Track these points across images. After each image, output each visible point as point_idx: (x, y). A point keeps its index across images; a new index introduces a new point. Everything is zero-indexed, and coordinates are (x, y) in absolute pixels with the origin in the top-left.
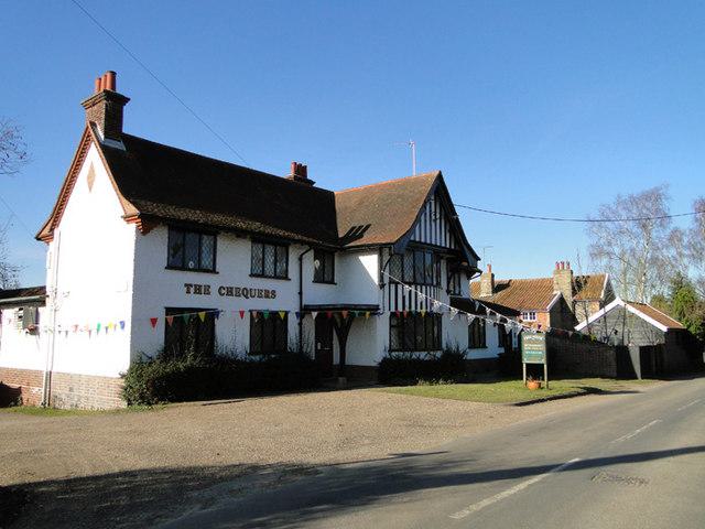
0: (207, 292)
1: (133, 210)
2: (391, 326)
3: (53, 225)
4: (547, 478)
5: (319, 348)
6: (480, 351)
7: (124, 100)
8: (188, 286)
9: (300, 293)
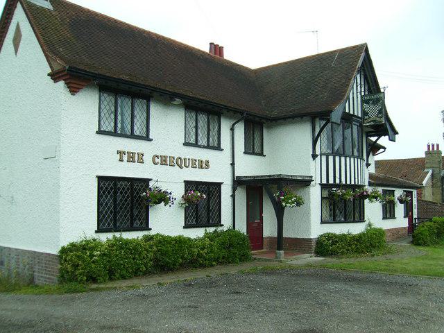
0: (141, 161)
9: (233, 164)
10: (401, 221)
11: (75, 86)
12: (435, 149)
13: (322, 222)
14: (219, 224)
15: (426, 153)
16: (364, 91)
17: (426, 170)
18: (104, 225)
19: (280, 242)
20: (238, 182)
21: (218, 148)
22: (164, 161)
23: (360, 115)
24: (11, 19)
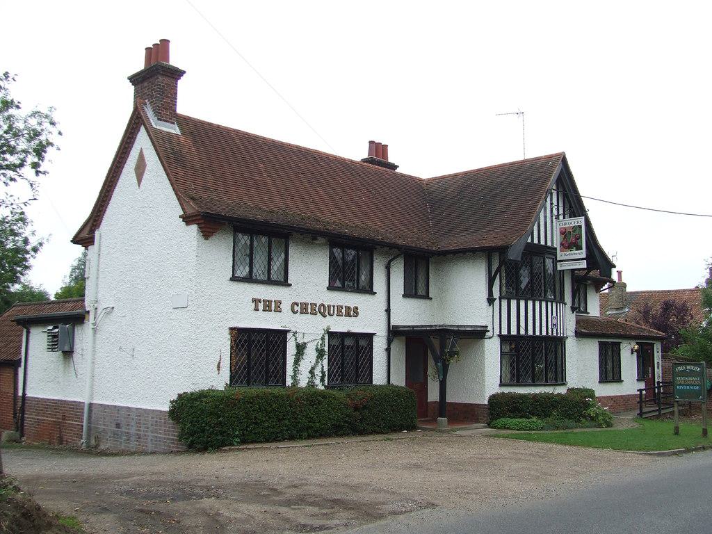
0: (278, 310)
4: (36, 394)
6: (375, 339)
7: (177, 74)
8: (256, 301)
9: (388, 311)
10: (630, 384)
11: (209, 230)
20: (394, 333)
21: (369, 290)
22: (302, 308)
24: (133, 143)
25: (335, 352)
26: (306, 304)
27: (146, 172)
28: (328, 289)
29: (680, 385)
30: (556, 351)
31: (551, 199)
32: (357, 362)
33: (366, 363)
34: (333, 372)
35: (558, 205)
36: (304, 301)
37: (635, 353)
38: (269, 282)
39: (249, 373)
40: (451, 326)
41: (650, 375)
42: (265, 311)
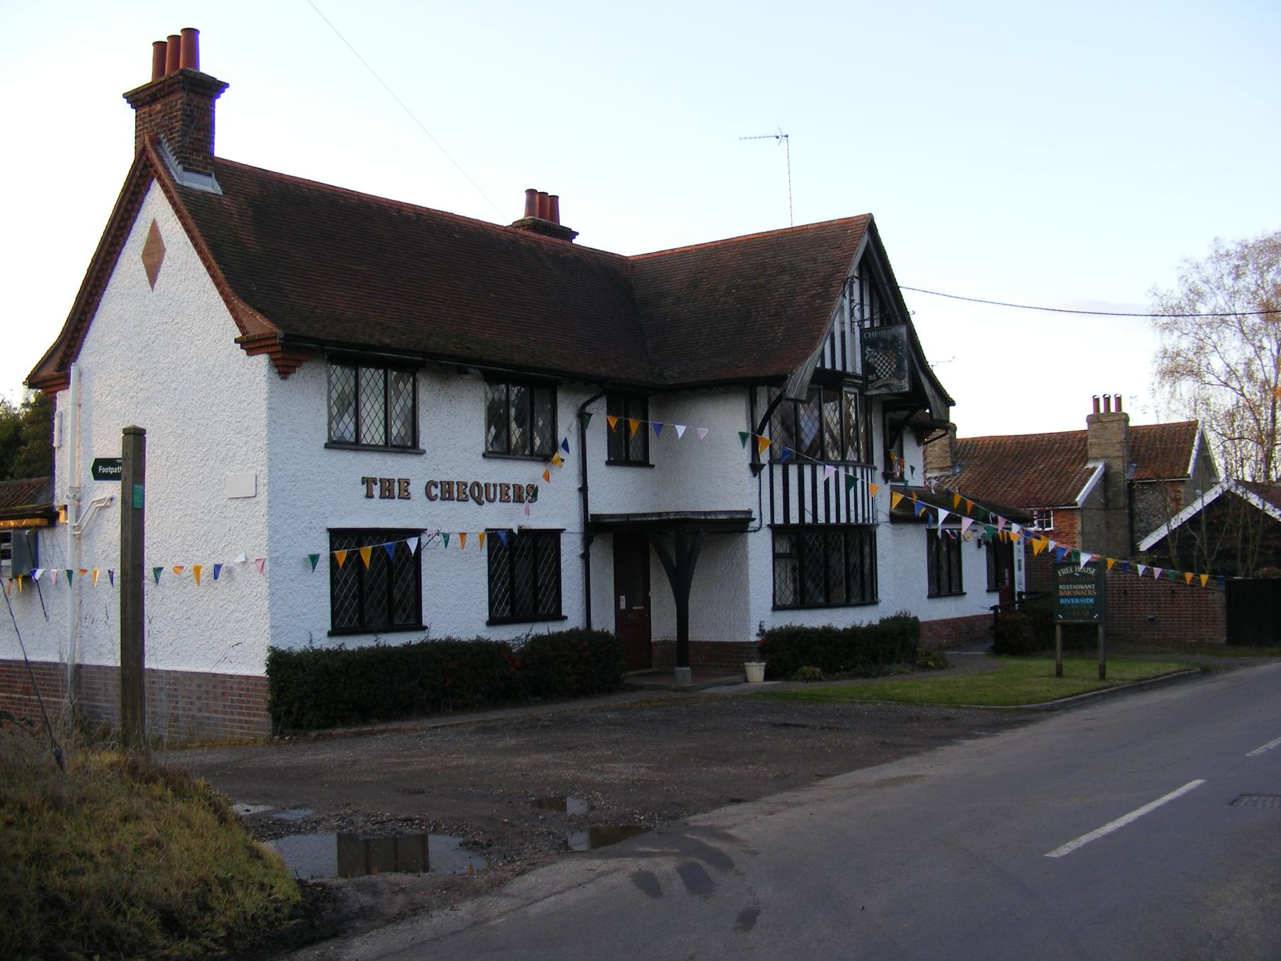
1: (261, 325)
2: (776, 556)
3: (65, 354)
5: (623, 606)
6: (564, 539)
7: (215, 88)
8: (368, 482)
9: (584, 490)
12: (1113, 409)
13: (776, 608)
14: (558, 616)
15: (1091, 420)
16: (872, 319)
17: (1090, 466)
18: (342, 620)
19: (683, 649)
20: (594, 527)
22: (446, 491)
23: (859, 371)
25: (499, 563)
26: (450, 484)
27: (166, 263)
28: (484, 455)
29: (1065, 597)
30: (862, 550)
31: (851, 294)
32: (535, 582)
33: (550, 582)
34: (497, 597)
35: (862, 304)
36: (445, 478)
37: (984, 547)
38: (389, 447)
39: (361, 605)
40: (693, 513)
41: (1007, 581)
42: (385, 498)
